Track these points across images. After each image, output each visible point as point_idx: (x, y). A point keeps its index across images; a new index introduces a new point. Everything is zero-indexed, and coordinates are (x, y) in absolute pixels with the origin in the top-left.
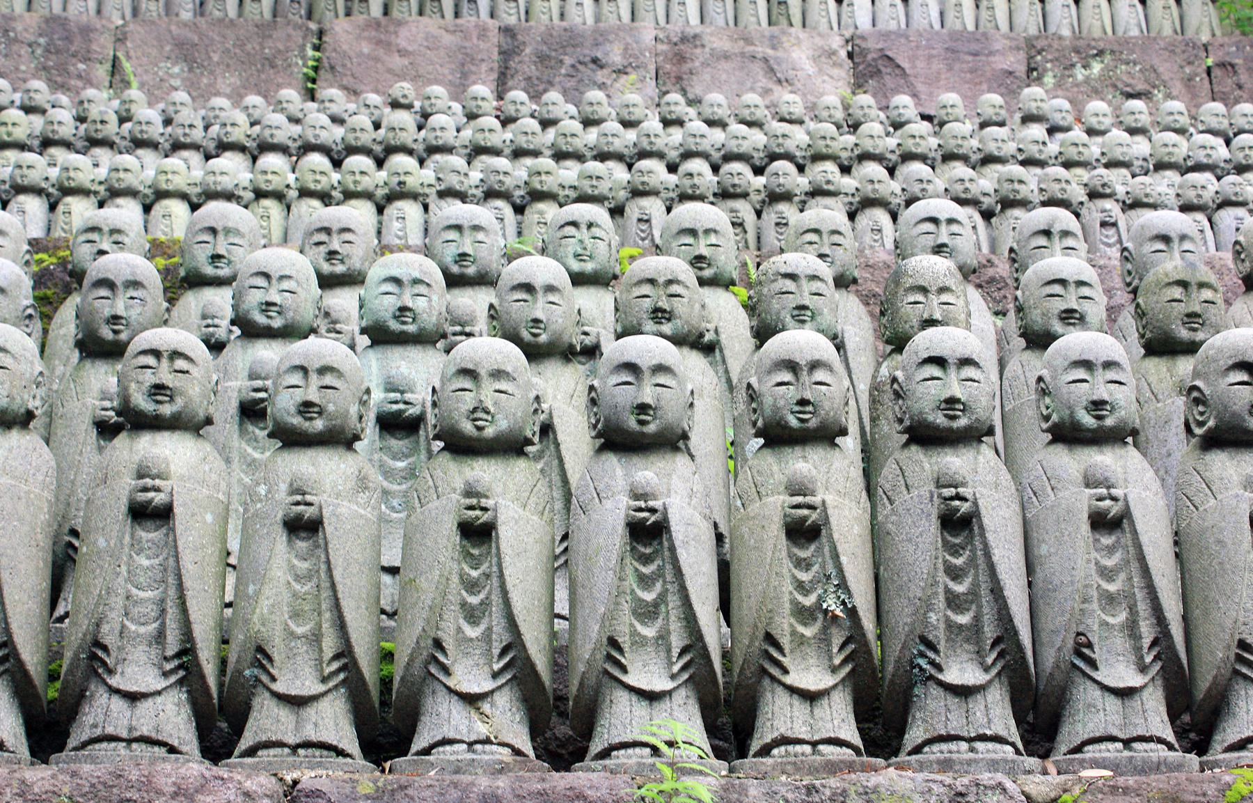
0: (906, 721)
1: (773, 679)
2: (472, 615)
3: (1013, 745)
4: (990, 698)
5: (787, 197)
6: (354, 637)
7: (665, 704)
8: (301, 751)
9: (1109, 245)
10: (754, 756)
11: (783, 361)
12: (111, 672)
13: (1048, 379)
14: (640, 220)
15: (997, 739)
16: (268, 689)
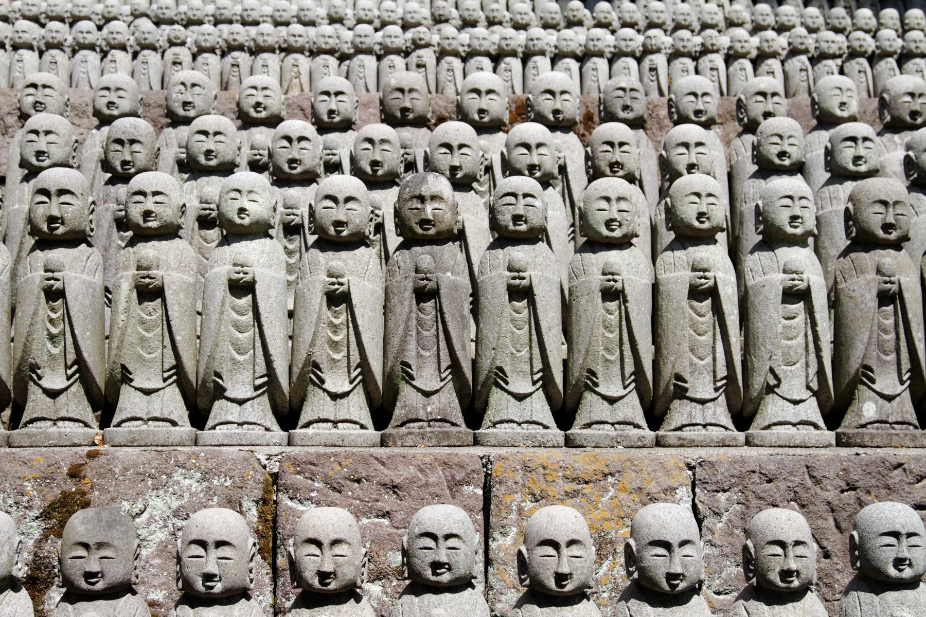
0: (846, 410)
2: (334, 345)
5: (59, 46)
8: (150, 422)
9: (652, 81)
10: (115, 426)
12: (413, 379)
14: (448, 70)
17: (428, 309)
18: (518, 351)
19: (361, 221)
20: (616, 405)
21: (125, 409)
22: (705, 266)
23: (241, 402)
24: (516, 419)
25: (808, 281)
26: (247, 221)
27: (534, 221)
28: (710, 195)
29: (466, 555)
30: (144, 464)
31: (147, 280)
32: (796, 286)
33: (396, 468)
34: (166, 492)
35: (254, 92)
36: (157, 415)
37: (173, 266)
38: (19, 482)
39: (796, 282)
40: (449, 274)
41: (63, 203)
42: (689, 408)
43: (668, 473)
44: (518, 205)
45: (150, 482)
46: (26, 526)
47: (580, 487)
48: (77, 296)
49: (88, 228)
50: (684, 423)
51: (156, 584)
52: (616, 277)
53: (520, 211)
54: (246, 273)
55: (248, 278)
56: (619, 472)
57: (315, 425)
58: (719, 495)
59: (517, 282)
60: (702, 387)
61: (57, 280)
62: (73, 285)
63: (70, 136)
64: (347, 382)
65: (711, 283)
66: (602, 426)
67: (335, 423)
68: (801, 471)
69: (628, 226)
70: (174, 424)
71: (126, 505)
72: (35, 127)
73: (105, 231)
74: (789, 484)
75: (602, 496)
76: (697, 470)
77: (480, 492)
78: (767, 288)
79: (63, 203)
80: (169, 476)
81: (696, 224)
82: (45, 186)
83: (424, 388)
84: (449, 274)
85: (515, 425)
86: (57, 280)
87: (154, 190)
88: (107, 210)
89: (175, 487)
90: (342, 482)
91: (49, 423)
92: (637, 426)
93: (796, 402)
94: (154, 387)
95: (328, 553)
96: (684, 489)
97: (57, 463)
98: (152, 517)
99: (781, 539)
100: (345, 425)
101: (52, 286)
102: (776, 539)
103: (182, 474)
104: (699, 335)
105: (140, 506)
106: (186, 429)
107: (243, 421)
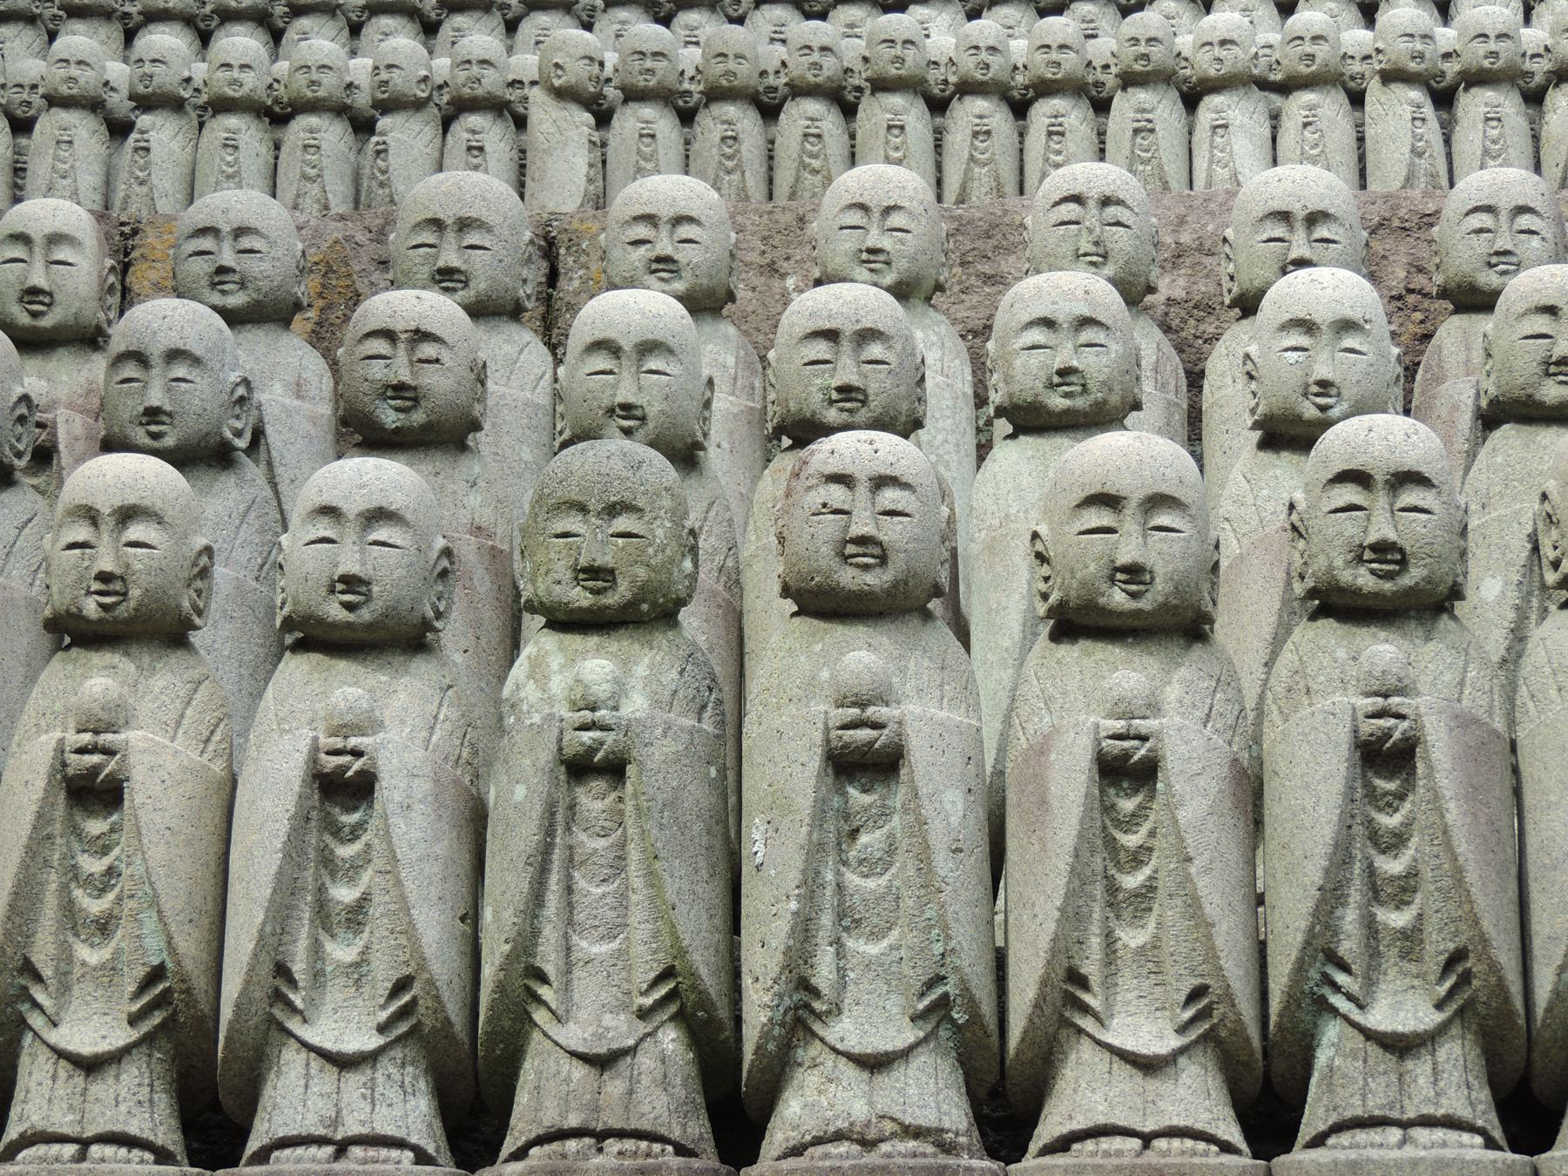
3: (1481, 1132)
4: (1442, 1054)
11: (80, 507)
13: (1301, 506)
15: (1451, 1123)
59: (864, 734)
67: (1147, 1139)
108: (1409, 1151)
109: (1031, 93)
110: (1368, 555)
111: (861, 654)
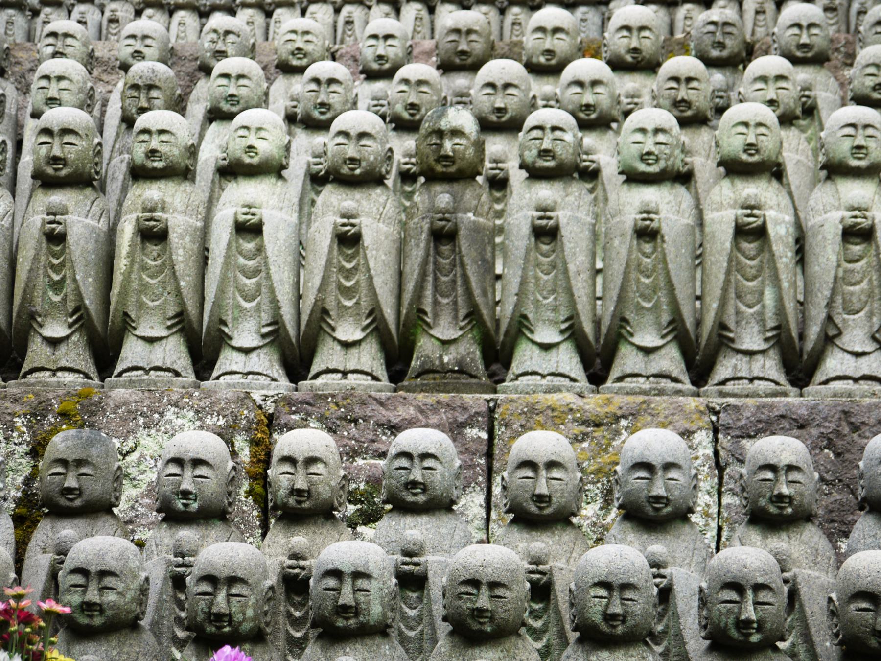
1: (35, 330)
6: (580, 307)
7: (554, 351)
8: (152, 372)
10: (116, 376)
16: (331, 336)
17: (447, 253)
18: (545, 298)
19: (376, 159)
20: (652, 357)
21: (127, 358)
22: (753, 203)
23: (247, 351)
24: (540, 371)
25: (873, 219)
26: (256, 160)
27: (563, 157)
28: (760, 125)
29: (443, 476)
30: (136, 402)
31: (152, 223)
32: (860, 224)
33: (395, 409)
34: (158, 431)
35: (292, 36)
36: (159, 364)
37: (179, 209)
38: (9, 418)
39: (859, 220)
40: (470, 215)
41: (66, 144)
42: (734, 361)
43: (688, 417)
44: (545, 139)
45: (142, 421)
46: (15, 462)
47: (590, 429)
48: (79, 240)
49: (93, 171)
50: (728, 376)
51: (144, 523)
52: (652, 216)
53: (546, 144)
54: (253, 215)
55: (255, 219)
56: (633, 414)
57: (324, 376)
58: (744, 441)
59: (544, 222)
60: (751, 339)
61: (59, 223)
62: (75, 229)
63: (85, 83)
64: (359, 330)
65: (760, 222)
66: (635, 379)
67: (345, 373)
68: (837, 416)
69: (667, 160)
70: (177, 374)
71: (117, 442)
72: (47, 73)
73: (120, 183)
74: (822, 430)
75: (613, 439)
76: (721, 415)
77: (484, 436)
78: (825, 227)
79: (66, 144)
80: (162, 415)
81: (744, 157)
82: (48, 126)
83: (441, 337)
84: (470, 215)
85: (539, 377)
86: (59, 223)
87: (160, 128)
88: (122, 161)
89: (167, 426)
90: (338, 422)
91: (48, 373)
92: (676, 380)
93: (858, 355)
94: (156, 335)
95: (301, 471)
96: (704, 433)
97: (48, 400)
98: (142, 456)
99: (772, 462)
100: (355, 376)
101: (54, 229)
102: (767, 462)
103: (174, 413)
104: (748, 280)
105: (130, 443)
106: (190, 377)
107: (250, 371)
108: (54, 379)
109: (142, 6)
110: (348, 162)
111: (545, 192)
